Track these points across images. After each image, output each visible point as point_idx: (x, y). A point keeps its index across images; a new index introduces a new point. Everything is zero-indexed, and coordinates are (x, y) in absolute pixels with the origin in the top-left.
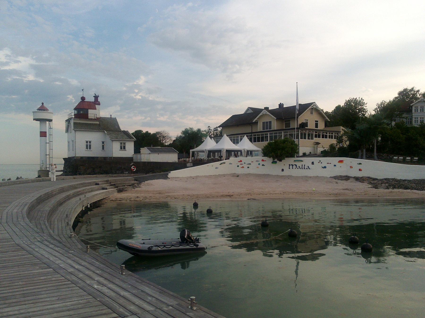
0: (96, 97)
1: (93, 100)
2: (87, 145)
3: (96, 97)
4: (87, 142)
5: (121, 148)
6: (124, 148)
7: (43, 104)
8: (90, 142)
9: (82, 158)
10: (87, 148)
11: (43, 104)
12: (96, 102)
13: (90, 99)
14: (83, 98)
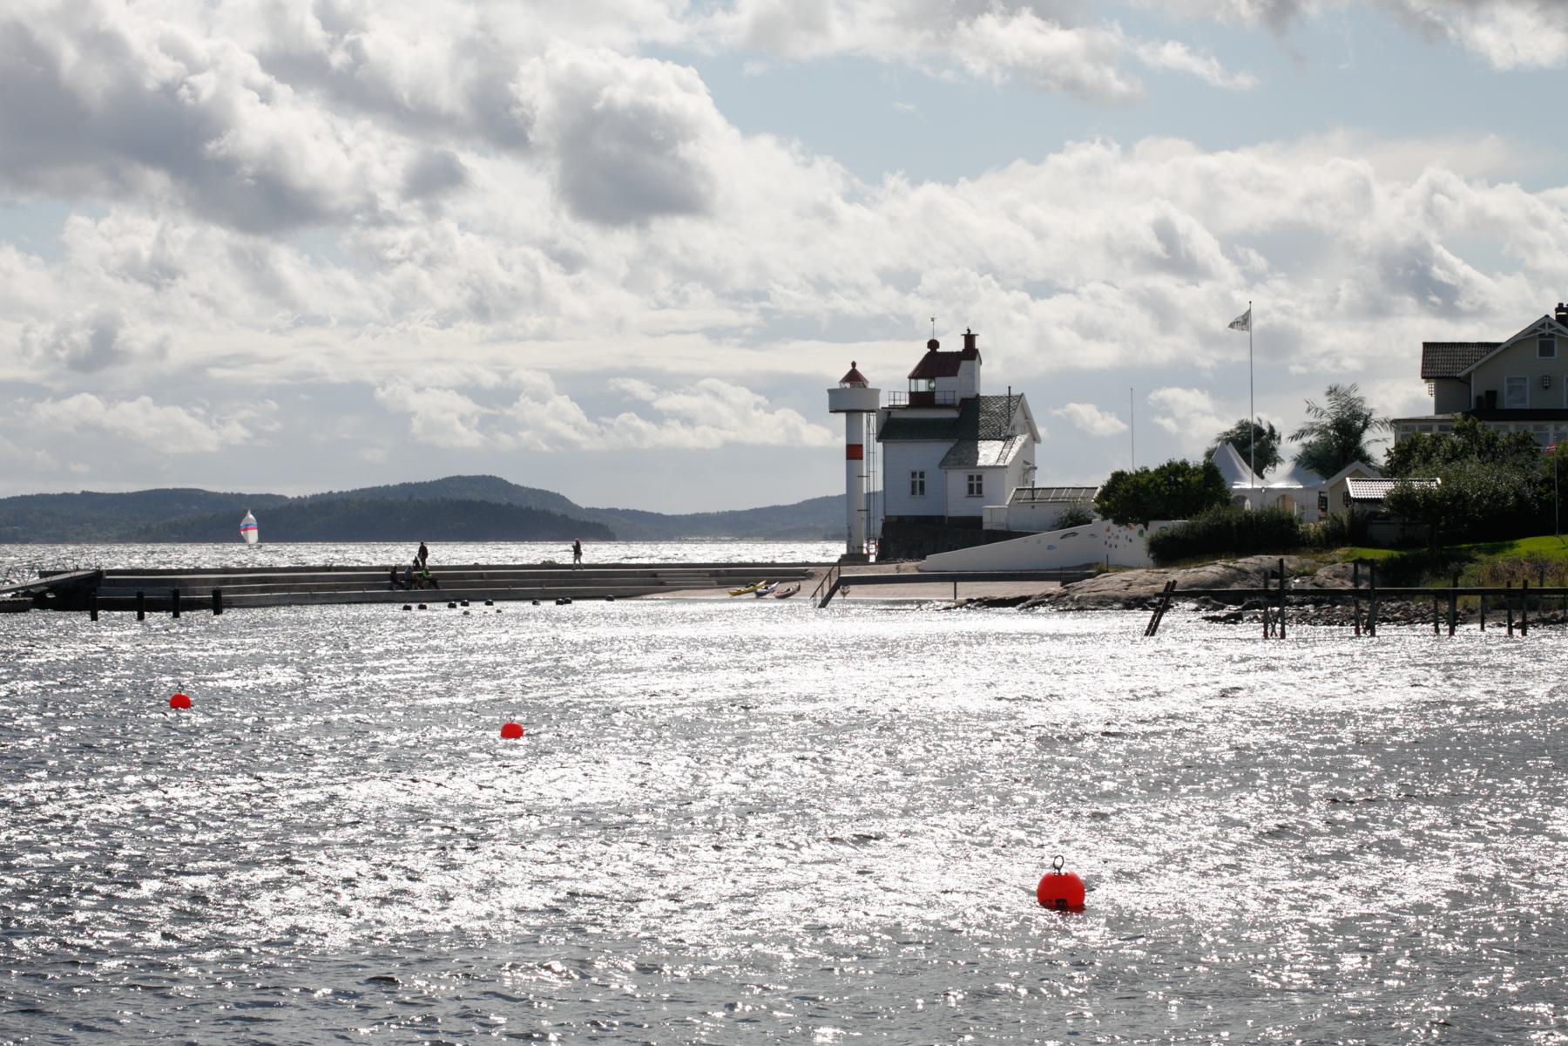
0: (970, 339)
1: (958, 345)
2: (971, 486)
3: (970, 339)
4: (914, 474)
5: (971, 491)
6: (980, 492)
7: (854, 364)
8: (922, 475)
9: (901, 518)
10: (913, 493)
11: (854, 364)
12: (971, 351)
13: (952, 344)
14: (933, 344)
